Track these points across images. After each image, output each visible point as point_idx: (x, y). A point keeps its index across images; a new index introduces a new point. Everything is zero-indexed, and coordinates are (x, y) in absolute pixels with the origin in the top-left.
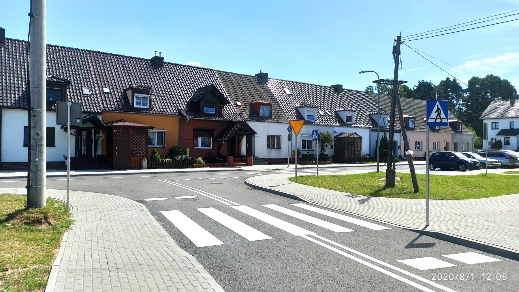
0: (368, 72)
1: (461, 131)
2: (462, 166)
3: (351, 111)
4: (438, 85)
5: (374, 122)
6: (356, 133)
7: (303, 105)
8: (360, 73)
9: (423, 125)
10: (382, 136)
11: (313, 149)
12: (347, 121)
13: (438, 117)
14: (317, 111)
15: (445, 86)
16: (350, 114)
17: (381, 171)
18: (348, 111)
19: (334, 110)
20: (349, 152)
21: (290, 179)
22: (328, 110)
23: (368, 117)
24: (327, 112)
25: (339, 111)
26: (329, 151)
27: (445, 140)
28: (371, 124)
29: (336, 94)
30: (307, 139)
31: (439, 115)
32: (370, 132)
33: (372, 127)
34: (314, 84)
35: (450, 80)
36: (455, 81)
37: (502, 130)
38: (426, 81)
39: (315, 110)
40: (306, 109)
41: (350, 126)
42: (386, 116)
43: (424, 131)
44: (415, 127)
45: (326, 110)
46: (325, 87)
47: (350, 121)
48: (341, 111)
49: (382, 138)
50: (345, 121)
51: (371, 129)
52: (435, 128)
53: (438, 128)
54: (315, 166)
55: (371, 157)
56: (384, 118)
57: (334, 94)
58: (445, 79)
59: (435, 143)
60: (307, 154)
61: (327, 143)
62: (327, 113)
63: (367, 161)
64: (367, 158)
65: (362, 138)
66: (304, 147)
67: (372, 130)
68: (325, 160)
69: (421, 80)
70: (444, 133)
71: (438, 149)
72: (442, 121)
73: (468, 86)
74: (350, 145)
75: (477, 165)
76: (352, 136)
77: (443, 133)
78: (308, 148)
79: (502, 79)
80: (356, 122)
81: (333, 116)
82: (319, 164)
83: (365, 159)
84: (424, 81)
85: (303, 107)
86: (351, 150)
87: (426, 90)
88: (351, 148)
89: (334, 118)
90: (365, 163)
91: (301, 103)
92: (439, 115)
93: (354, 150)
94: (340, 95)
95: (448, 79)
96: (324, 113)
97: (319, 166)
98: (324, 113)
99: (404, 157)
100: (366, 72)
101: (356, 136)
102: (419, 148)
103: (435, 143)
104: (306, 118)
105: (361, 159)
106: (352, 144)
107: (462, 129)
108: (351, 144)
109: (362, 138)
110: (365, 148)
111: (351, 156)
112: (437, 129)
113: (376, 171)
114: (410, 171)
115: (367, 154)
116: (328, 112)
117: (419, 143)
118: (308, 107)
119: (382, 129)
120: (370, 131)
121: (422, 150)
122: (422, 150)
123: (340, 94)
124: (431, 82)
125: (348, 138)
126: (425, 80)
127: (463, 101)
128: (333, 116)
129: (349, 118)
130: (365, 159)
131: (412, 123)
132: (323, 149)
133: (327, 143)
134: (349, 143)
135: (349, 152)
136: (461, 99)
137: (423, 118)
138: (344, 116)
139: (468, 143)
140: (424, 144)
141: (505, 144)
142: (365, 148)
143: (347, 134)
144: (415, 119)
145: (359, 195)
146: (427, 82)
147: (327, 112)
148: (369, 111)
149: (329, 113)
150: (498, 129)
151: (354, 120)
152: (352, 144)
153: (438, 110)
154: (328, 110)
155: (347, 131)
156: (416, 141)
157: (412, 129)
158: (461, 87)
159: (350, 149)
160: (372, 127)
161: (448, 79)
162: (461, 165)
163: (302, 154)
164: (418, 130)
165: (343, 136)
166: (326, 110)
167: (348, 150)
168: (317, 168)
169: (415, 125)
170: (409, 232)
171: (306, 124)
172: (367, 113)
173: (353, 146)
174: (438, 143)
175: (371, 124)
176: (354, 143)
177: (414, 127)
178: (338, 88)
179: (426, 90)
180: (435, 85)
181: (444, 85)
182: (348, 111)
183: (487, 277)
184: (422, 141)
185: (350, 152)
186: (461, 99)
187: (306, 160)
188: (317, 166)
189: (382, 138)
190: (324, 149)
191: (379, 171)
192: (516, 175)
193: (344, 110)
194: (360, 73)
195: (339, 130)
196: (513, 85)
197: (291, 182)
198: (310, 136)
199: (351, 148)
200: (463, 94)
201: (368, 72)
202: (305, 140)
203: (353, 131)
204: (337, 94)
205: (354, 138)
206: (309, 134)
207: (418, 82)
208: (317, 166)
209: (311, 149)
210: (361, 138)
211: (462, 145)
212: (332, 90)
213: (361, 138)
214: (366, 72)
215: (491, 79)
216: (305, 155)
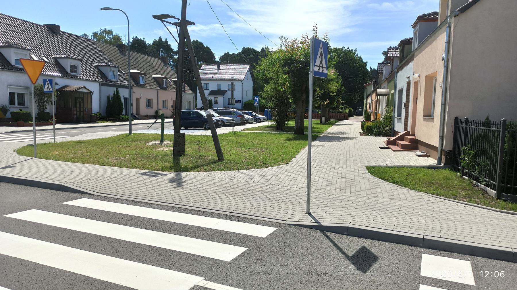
0: (113, 9)
1: (185, 90)
2: (207, 124)
3: (75, 59)
4: (151, 44)
5: (103, 76)
6: (85, 87)
7: (8, 45)
8: (102, 9)
9: (152, 82)
10: (115, 92)
11: (26, 105)
12: (71, 71)
13: (48, 88)
14: (30, 55)
15: (158, 46)
16: (74, 63)
17: (138, 132)
18: (71, 58)
19: (53, 57)
20: (77, 110)
21: (20, 152)
22: (43, 55)
23: (95, 69)
24: (43, 57)
25: (59, 58)
26: (51, 109)
27: (172, 98)
28: (100, 77)
29: (52, 36)
30: (16, 91)
31: (48, 87)
32: (99, 87)
33: (101, 80)
34: (19, 18)
35: (162, 40)
36: (166, 42)
37: (212, 91)
38: (140, 39)
39: (26, 53)
40: (12, 50)
41: (75, 77)
42: (117, 69)
43: (154, 89)
44: (145, 83)
45: (41, 55)
46: (36, 24)
47: (75, 72)
48: (62, 58)
49: (114, 93)
50: (69, 71)
51: (100, 83)
52: (163, 86)
53: (166, 86)
54: (31, 128)
55: (102, 115)
56: (113, 72)
57: (50, 35)
58: (157, 39)
59: (164, 101)
60: (19, 113)
61: (47, 98)
62: (42, 59)
63: (98, 120)
64: (98, 117)
65: (92, 93)
66: (12, 102)
67: (102, 84)
68: (47, 120)
69: (135, 37)
70: (172, 91)
71: (166, 107)
72: (50, 90)
73: (178, 48)
74: (78, 102)
75: (220, 123)
76: (80, 90)
77: (170, 91)
78: (19, 104)
79: (205, 46)
80: (82, 74)
81: (52, 64)
82: (37, 125)
83: (97, 118)
84: (138, 38)
85: (7, 47)
86: (80, 107)
87: (141, 47)
88: (80, 105)
89: (53, 65)
90: (98, 123)
91: (3, 42)
92: (48, 87)
93: (83, 108)
94: (58, 38)
95: (160, 39)
96: (40, 59)
97: (37, 128)
98: (40, 59)
99: (137, 115)
100: (110, 9)
101: (85, 90)
102: (149, 106)
103: (164, 101)
104: (13, 63)
105: (92, 119)
106: (81, 100)
107: (185, 88)
108: (79, 100)
109: (92, 93)
110: (96, 106)
111: (80, 114)
112: (164, 87)
113: (128, 132)
114: (174, 133)
115: (98, 113)
116: (44, 58)
117: (149, 100)
118: (16, 47)
119: (113, 84)
120: (99, 85)
121: (152, 108)
122: (152, 108)
123: (58, 37)
124: (145, 40)
125: (75, 92)
126: (139, 37)
127: (173, 62)
128: (52, 64)
129: (74, 68)
130: (97, 118)
131: (143, 79)
132: (41, 105)
133: (47, 98)
134: (76, 99)
135: (77, 110)
136: (172, 60)
137: (151, 75)
138: (67, 65)
139: (190, 102)
140: (155, 102)
141: (214, 104)
142: (96, 106)
143: (73, 88)
144: (145, 74)
145: (157, 171)
146: (140, 39)
147: (43, 57)
148: (96, 62)
149: (46, 60)
150: (209, 90)
151: (79, 70)
152: (81, 100)
153: (48, 84)
154: (43, 55)
155: (73, 85)
156: (147, 99)
157: (143, 86)
158: (172, 48)
159: (78, 105)
160: (101, 80)
161: (160, 39)
162: (206, 124)
163: (11, 113)
164: (149, 87)
165: (68, 90)
166: (41, 55)
167: (76, 107)
168: (54, 129)
169: (145, 82)
170: (304, 229)
171: (14, 72)
172: (94, 64)
173: (82, 102)
174: (166, 101)
175: (100, 77)
176: (83, 99)
177: (144, 84)
178: (54, 29)
179: (141, 47)
180: (148, 44)
181: (157, 45)
182: (71, 58)
183: (484, 274)
184: (152, 99)
185: (78, 110)
186: (172, 60)
187: (18, 120)
188: (54, 127)
189: (114, 93)
190: (44, 105)
191: (132, 132)
192: (248, 132)
193: (67, 57)
194: (102, 9)
195: (62, 82)
196: (213, 52)
197: (24, 158)
198: (21, 88)
199: (80, 105)
200: (174, 55)
201: (113, 9)
202: (14, 94)
203: (81, 84)
204: (54, 36)
205: (83, 93)
206: (19, 85)
207: (132, 38)
208: (54, 127)
209: (24, 105)
210: (91, 93)
211: (186, 105)
212: (46, 30)
213: (91, 93)
214: (110, 9)
215: (196, 44)
216: (17, 113)
